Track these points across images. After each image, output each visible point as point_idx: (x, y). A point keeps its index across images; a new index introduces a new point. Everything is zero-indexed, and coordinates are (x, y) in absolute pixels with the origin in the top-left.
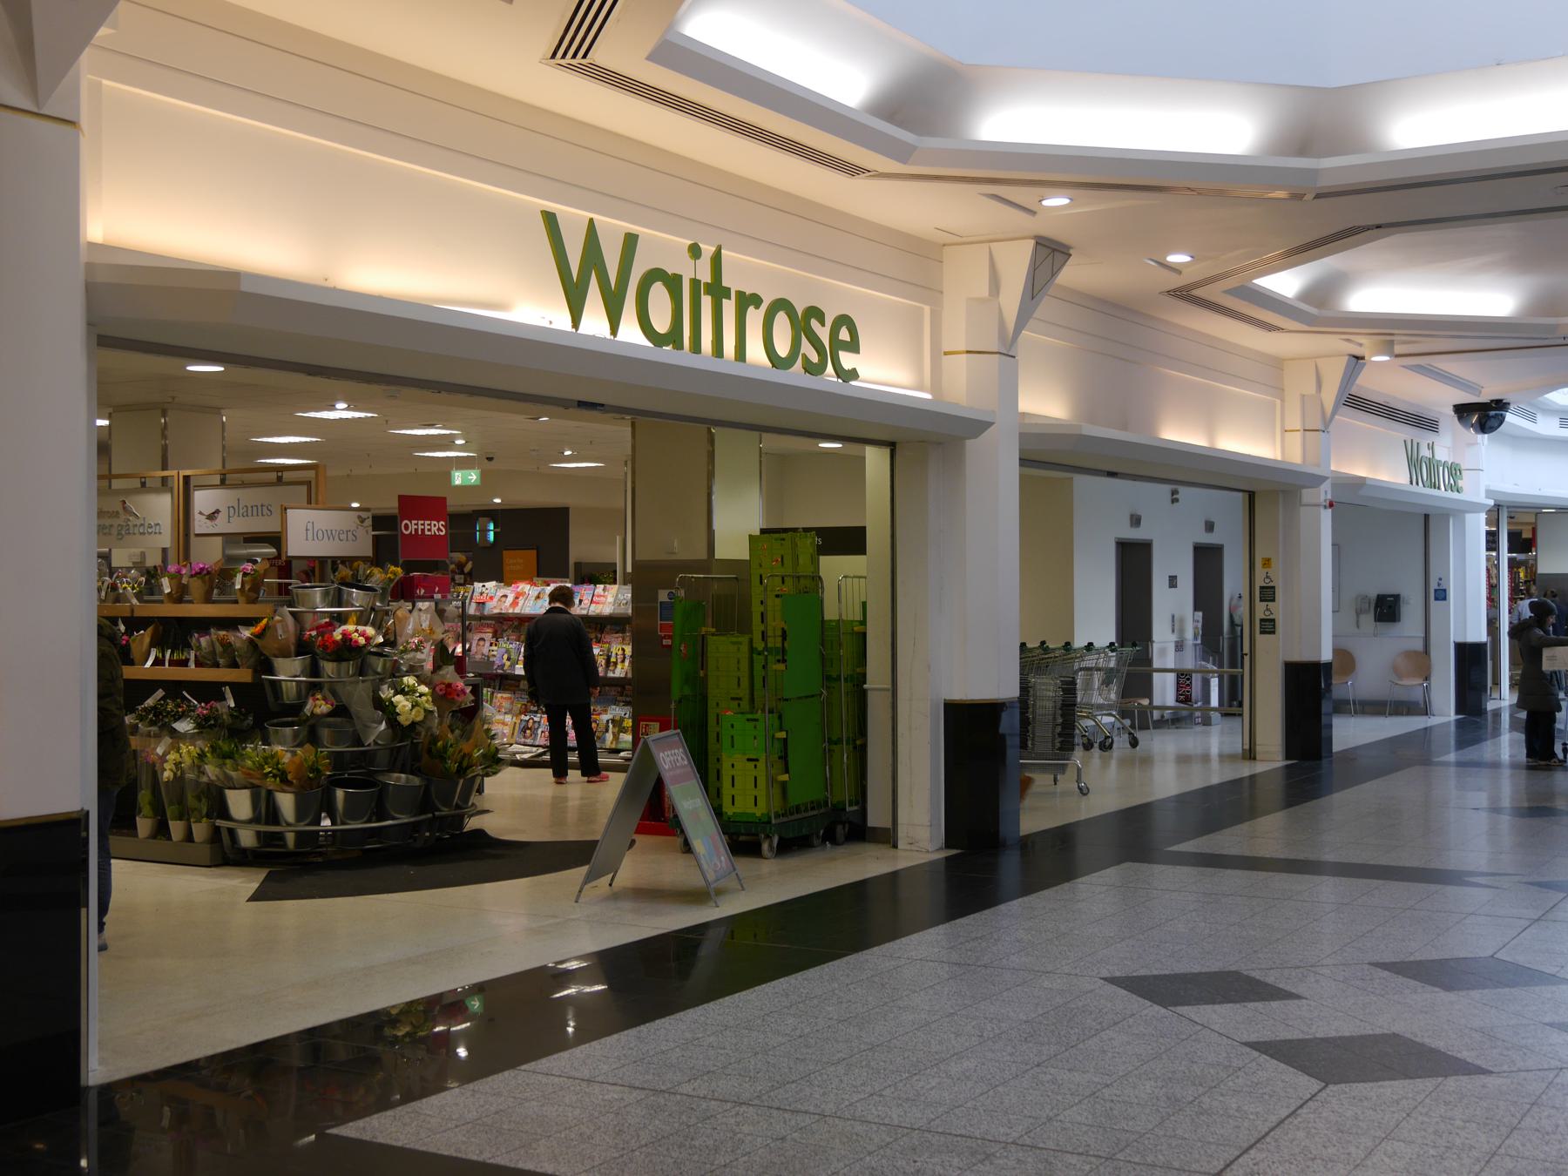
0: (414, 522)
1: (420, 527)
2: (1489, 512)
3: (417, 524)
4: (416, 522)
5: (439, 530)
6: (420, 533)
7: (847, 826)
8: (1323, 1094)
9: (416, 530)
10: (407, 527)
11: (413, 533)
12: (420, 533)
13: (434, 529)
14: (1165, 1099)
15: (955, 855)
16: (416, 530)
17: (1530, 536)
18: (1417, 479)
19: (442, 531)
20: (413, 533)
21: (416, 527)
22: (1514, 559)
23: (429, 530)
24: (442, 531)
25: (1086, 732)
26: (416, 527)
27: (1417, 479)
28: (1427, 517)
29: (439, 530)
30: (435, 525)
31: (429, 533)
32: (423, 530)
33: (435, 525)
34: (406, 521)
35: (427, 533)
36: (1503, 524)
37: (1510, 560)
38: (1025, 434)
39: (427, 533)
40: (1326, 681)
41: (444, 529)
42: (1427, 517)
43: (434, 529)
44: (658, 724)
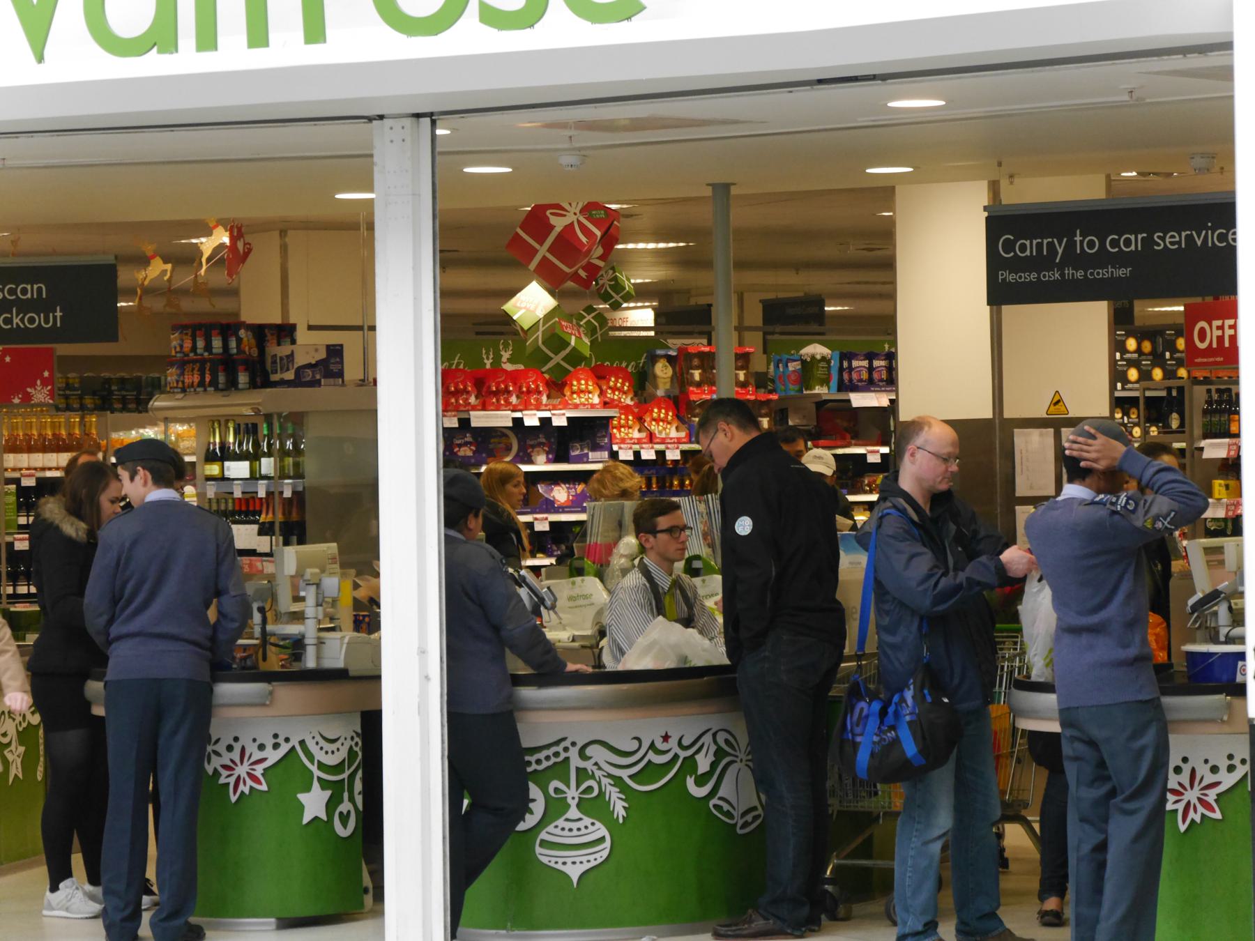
0: (1217, 323)
3: (1221, 328)
4: (1219, 323)
5: (1163, 239)
6: (1227, 344)
7: (258, 476)
8: (187, 451)
9: (1220, 339)
11: (1215, 345)
12: (1227, 344)
15: (78, 836)
16: (1220, 339)
18: (1187, 498)
19: (1159, 237)
20: (1215, 345)
21: (1220, 333)
22: (1014, 623)
24: (1159, 237)
25: (728, 814)
26: (1220, 333)
27: (1187, 498)
29: (1163, 239)
34: (1203, 324)
44: (27, 548)
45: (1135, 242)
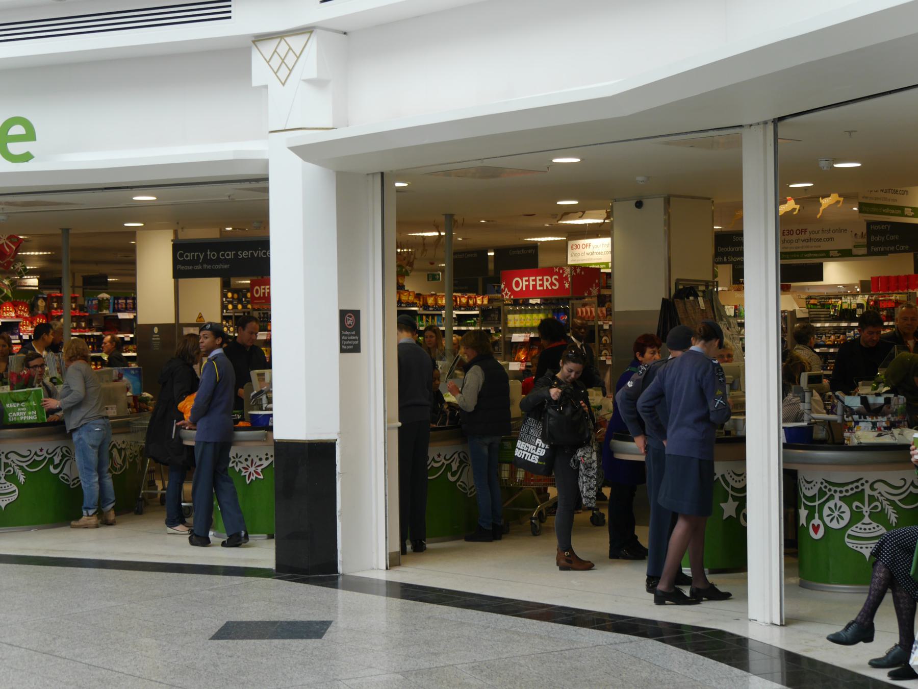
0: (524, 279)
1: (532, 283)
2: (665, 198)
6: (531, 289)
9: (528, 286)
10: (517, 284)
12: (531, 289)
13: (547, 284)
14: (678, 663)
17: (831, 255)
19: (555, 285)
21: (264, 291)
23: (541, 285)
24: (555, 285)
26: (264, 291)
28: (382, 174)
29: (552, 284)
30: (547, 280)
31: (542, 288)
32: (535, 286)
33: (547, 280)
35: (538, 288)
36: (591, 259)
37: (781, 285)
38: (783, 264)
39: (538, 288)
40: (598, 627)
41: (557, 284)
42: (382, 174)
43: (547, 284)
45: (231, 255)
